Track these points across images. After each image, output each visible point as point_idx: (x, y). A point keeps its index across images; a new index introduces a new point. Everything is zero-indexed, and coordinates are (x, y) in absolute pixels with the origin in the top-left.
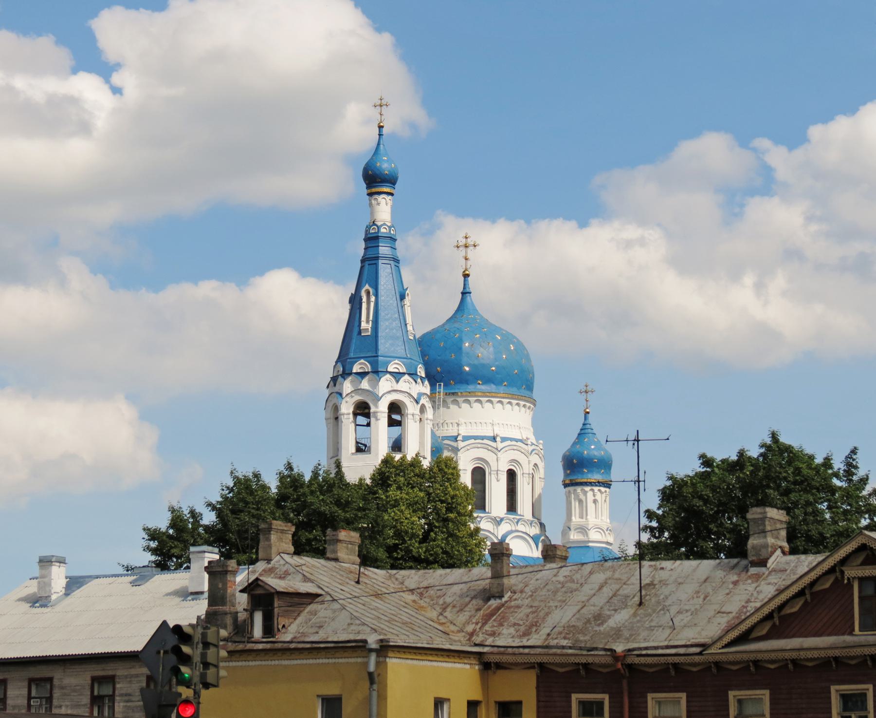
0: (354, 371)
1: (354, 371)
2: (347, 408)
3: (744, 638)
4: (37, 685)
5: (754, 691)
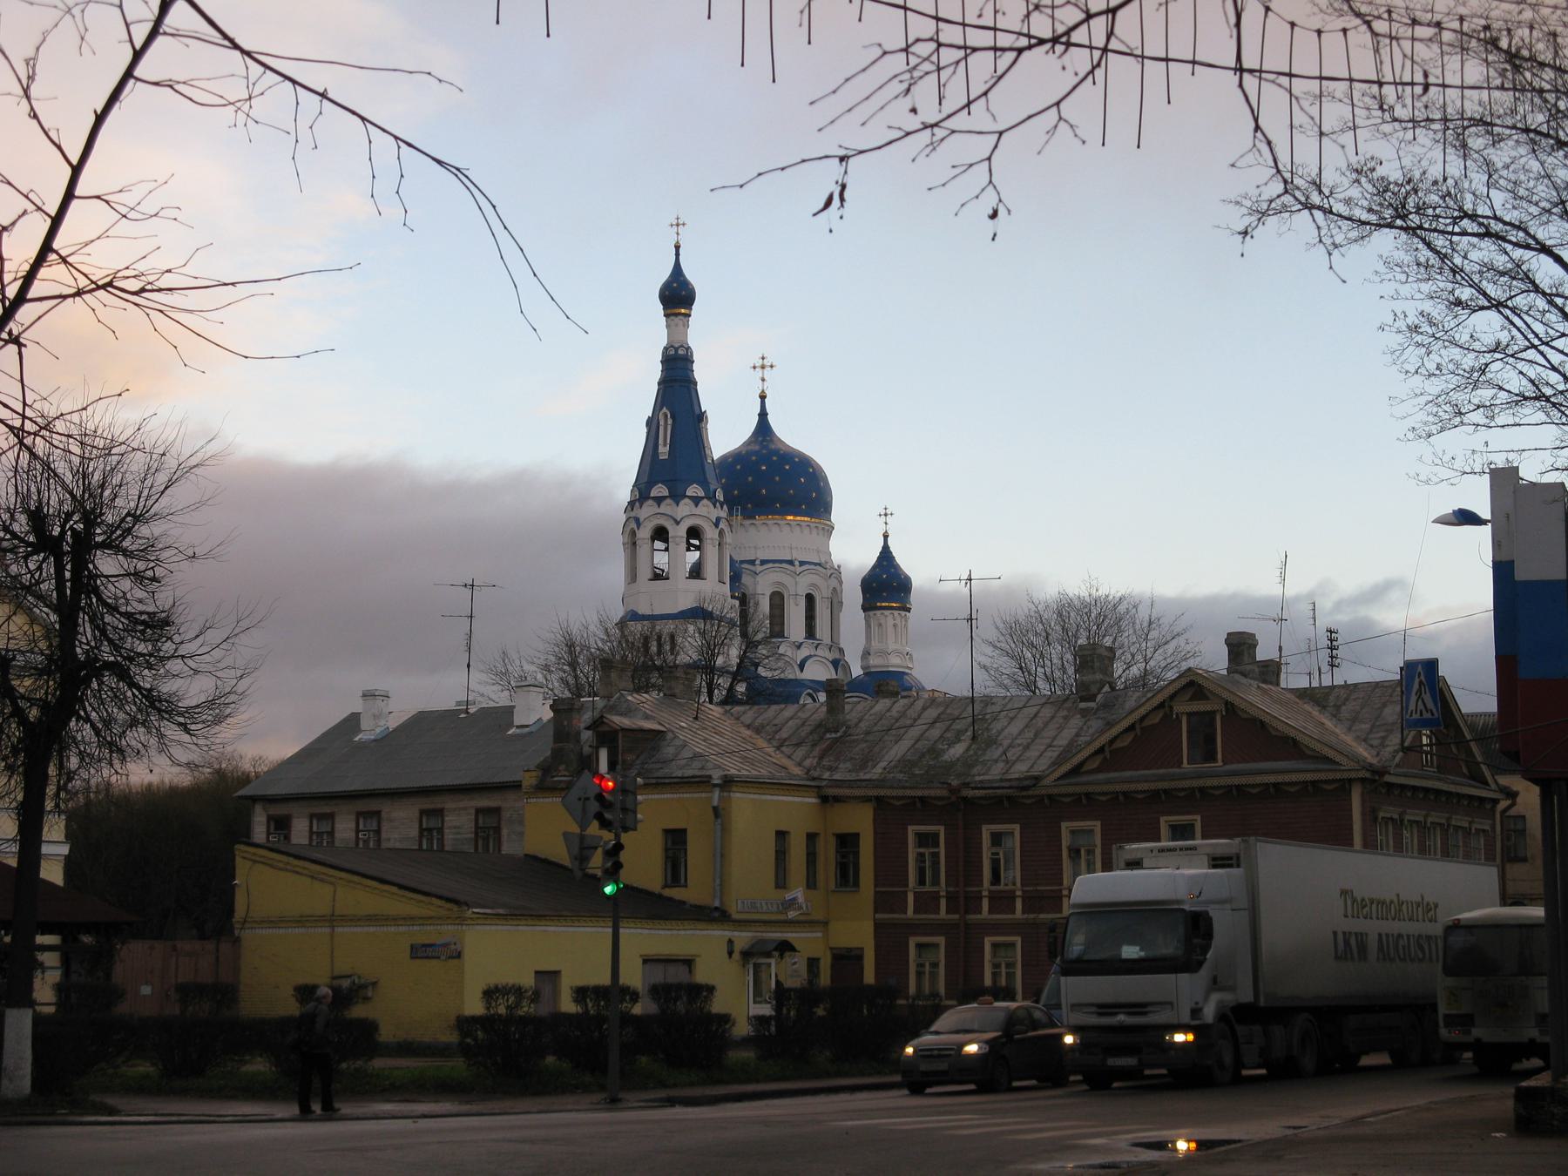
0: (652, 495)
1: (652, 495)
2: (645, 533)
3: (1076, 771)
4: (318, 820)
5: (1354, 832)
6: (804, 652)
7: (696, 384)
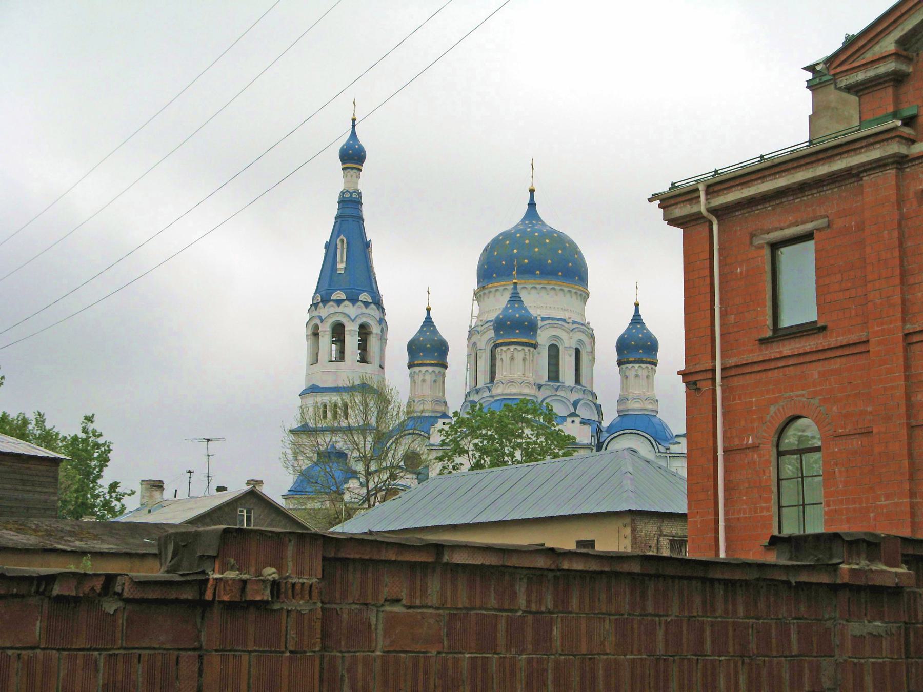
1: (332, 299)
6: (575, 397)
7: (363, 220)
